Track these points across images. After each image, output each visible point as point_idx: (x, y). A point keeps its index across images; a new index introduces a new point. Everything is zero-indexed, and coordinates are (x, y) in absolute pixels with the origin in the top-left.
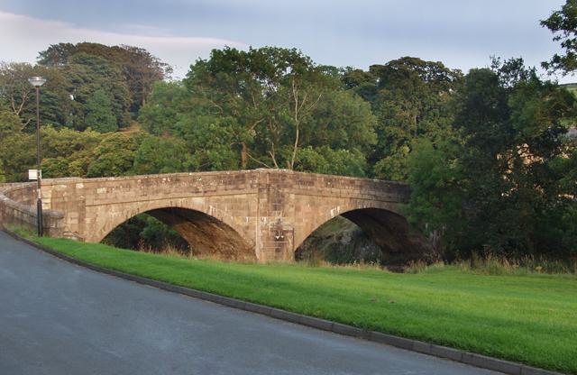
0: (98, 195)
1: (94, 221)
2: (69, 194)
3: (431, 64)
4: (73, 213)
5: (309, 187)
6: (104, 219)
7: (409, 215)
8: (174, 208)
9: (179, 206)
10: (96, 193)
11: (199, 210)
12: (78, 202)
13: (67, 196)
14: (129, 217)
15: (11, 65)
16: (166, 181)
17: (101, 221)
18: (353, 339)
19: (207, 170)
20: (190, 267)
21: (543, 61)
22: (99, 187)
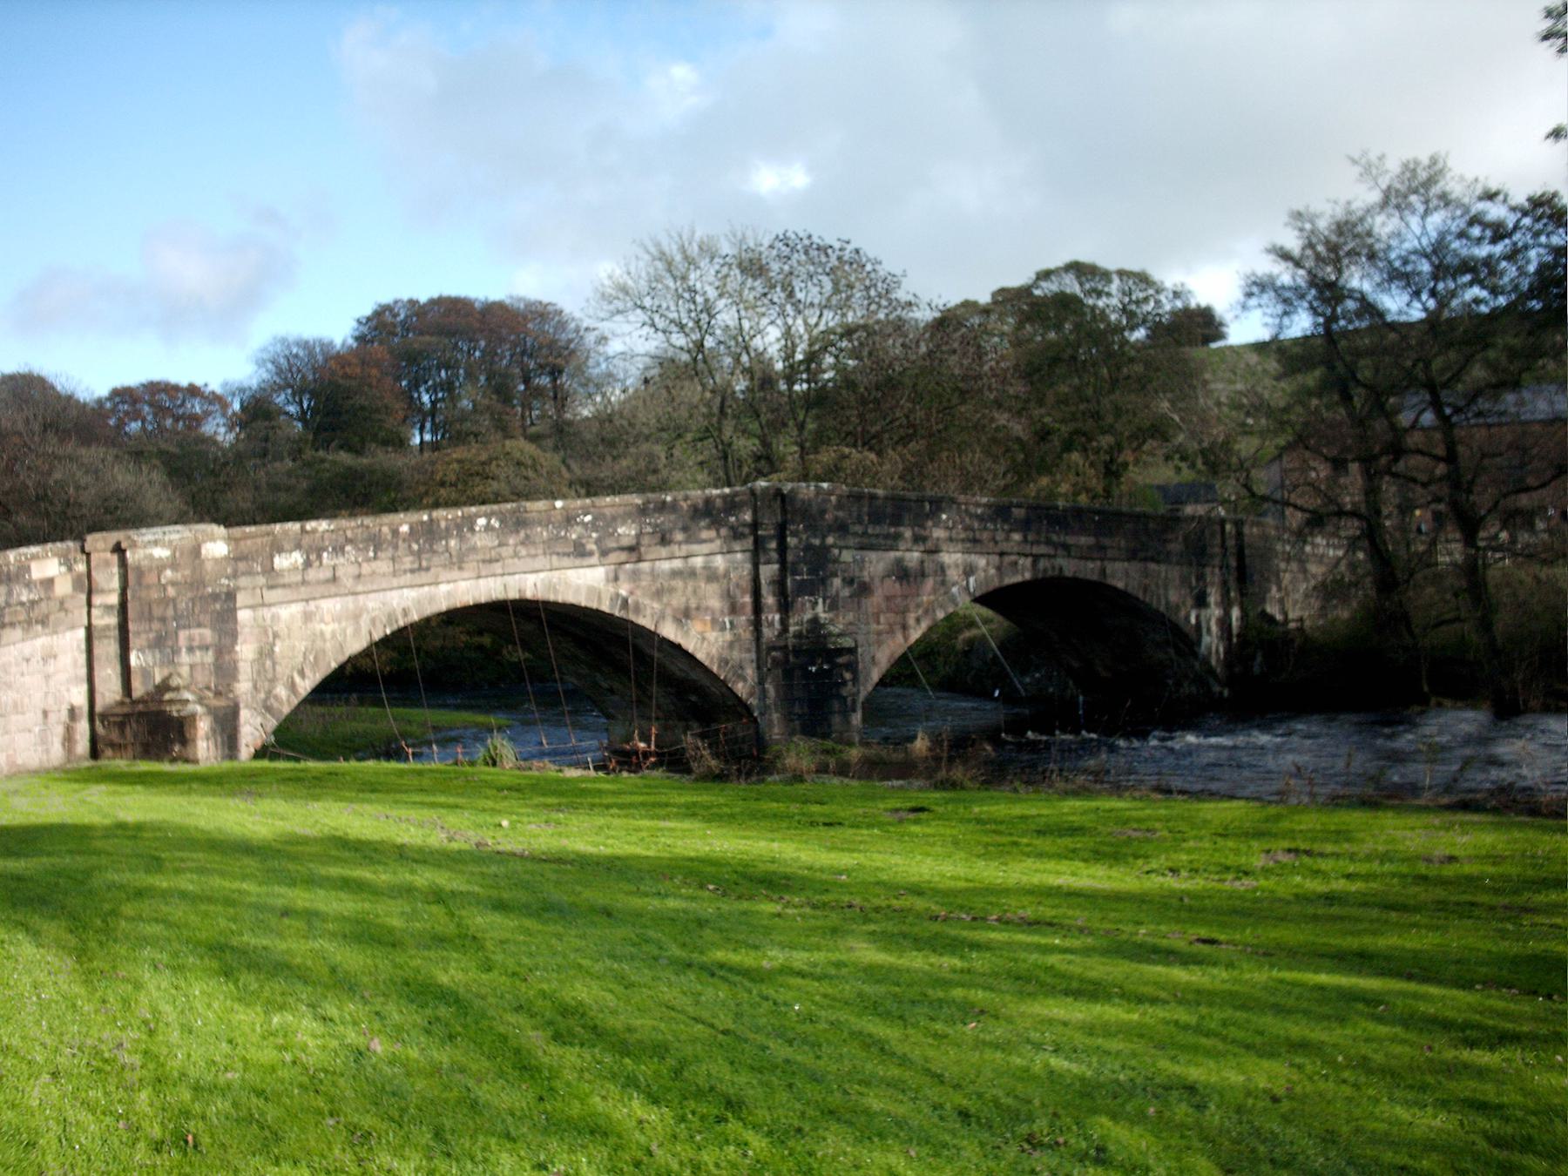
0: (280, 574)
1: (266, 654)
2: (179, 576)
3: (1122, 274)
4: (196, 632)
5: (892, 530)
6: (301, 646)
7: (844, 315)
8: (514, 602)
9: (529, 595)
10: (270, 570)
11: (583, 601)
12: (215, 597)
13: (174, 583)
14: (377, 636)
15: (298, 344)
16: (488, 528)
17: (291, 649)
18: (139, 788)
19: (1463, 987)
20: (1481, 1073)
21: (1299, 206)
22: (280, 550)
